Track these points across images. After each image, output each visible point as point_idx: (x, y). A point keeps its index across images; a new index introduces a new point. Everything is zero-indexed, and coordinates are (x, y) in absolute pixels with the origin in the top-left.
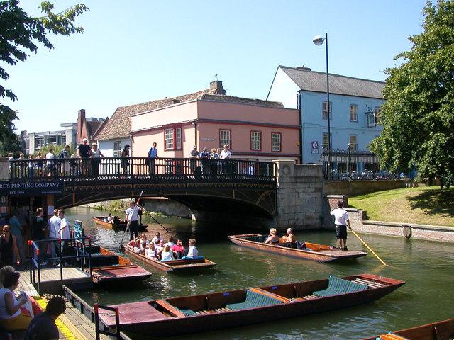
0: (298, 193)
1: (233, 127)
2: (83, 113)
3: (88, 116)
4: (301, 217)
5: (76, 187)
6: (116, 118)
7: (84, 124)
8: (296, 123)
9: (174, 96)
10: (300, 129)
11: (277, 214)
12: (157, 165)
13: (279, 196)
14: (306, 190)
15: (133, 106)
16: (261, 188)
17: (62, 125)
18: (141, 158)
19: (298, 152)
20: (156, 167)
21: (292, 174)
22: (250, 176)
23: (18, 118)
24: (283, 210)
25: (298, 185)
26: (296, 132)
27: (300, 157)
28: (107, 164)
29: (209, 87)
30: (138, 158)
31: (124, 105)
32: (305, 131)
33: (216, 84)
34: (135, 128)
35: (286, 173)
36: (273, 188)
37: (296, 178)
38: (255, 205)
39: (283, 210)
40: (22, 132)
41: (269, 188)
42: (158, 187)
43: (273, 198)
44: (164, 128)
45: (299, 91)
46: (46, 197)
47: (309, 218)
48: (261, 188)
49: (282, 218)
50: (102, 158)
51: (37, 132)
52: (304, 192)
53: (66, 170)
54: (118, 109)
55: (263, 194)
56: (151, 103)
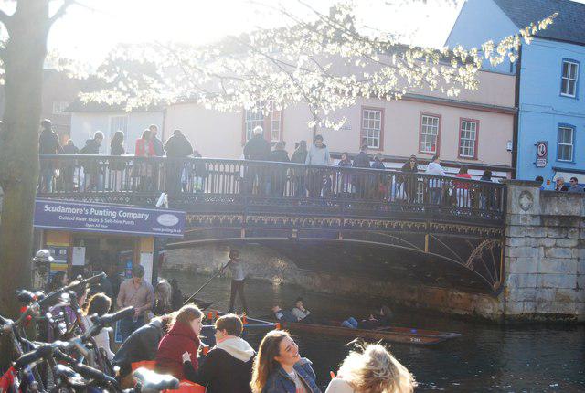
0: (545, 248)
4: (548, 295)
10: (515, 114)
13: (511, 252)
14: (560, 242)
21: (537, 210)
24: (516, 282)
25: (545, 231)
26: (509, 121)
35: (525, 205)
36: (498, 236)
37: (543, 217)
41: (491, 235)
47: (565, 300)
49: (512, 297)
52: (556, 246)
55: (481, 246)
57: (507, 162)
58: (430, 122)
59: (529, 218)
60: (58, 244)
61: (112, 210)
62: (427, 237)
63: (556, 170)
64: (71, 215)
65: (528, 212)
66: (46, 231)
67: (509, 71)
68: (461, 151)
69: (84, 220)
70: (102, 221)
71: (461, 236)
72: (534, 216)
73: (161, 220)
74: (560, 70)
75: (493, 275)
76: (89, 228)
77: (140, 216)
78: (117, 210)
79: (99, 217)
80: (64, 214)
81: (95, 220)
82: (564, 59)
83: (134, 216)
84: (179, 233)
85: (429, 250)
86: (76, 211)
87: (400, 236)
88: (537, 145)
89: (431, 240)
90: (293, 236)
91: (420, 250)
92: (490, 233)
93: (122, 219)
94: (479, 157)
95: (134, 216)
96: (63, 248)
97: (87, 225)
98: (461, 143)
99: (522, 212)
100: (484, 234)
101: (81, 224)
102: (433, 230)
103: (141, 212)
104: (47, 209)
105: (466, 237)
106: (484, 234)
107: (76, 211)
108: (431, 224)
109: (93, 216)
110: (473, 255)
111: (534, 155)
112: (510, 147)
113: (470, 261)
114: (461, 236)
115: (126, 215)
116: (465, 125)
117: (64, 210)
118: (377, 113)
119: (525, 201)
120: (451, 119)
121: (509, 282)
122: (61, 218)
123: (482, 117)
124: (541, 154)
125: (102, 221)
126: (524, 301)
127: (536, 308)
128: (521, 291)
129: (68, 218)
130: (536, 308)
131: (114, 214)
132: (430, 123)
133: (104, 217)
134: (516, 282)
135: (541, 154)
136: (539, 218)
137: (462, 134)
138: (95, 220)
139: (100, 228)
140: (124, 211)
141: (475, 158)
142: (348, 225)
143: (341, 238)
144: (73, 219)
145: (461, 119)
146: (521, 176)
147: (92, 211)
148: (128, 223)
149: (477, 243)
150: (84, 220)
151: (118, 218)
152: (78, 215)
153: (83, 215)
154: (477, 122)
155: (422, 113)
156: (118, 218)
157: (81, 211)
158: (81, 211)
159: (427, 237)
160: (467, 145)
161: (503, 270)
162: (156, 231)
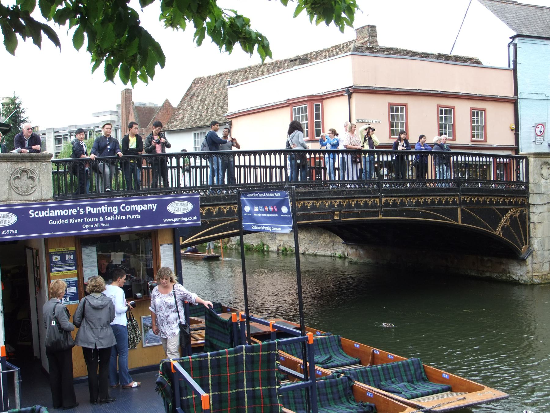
5: (384, 199)
7: (132, 111)
8: (509, 93)
9: (301, 53)
10: (514, 102)
11: (530, 252)
12: (239, 167)
13: (534, 218)
15: (220, 75)
16: (504, 203)
17: (97, 115)
19: (511, 142)
20: (169, 170)
27: (517, 150)
28: (195, 167)
31: (206, 75)
32: (522, 105)
33: (366, 31)
36: (523, 204)
38: (495, 236)
39: (542, 245)
41: (516, 204)
42: (332, 206)
43: (521, 226)
44: (289, 104)
45: (513, 38)
46: (311, 273)
48: (504, 203)
49: (539, 259)
50: (234, 153)
51: (57, 126)
53: (331, 161)
54: (195, 82)
55: (508, 214)
56: (250, 68)
57: (511, 142)
58: (445, 113)
61: (112, 205)
62: (459, 210)
64: (63, 217)
67: (507, 66)
70: (101, 219)
73: (173, 208)
75: (521, 240)
76: (87, 229)
77: (146, 207)
78: (118, 205)
79: (97, 215)
81: (93, 220)
83: (139, 208)
84: (195, 221)
86: (68, 212)
87: (436, 210)
88: (536, 127)
89: (462, 210)
90: (336, 218)
91: (454, 222)
92: (516, 202)
93: (125, 213)
94: (488, 140)
95: (139, 208)
96: (69, 253)
97: (84, 226)
98: (473, 129)
99: (543, 181)
100: (510, 203)
101: (78, 226)
102: (464, 202)
103: (147, 203)
104: (32, 214)
105: (493, 207)
106: (510, 203)
107: (68, 212)
109: (90, 215)
110: (502, 224)
111: (533, 134)
113: (499, 229)
114: (490, 207)
115: (129, 208)
117: (53, 213)
118: (402, 109)
120: (463, 110)
121: (536, 244)
122: (51, 222)
123: (488, 106)
129: (61, 222)
131: (115, 209)
132: (446, 114)
133: (103, 215)
135: (539, 134)
137: (473, 121)
138: (93, 220)
139: (101, 227)
141: (485, 141)
142: (387, 204)
143: (381, 217)
144: (66, 221)
145: (472, 109)
146: (522, 152)
147: (88, 209)
148: (132, 217)
151: (120, 213)
152: (72, 216)
153: (78, 216)
154: (405, 105)
156: (120, 213)
157: (74, 212)
158: (74, 212)
159: (459, 210)
161: (529, 236)
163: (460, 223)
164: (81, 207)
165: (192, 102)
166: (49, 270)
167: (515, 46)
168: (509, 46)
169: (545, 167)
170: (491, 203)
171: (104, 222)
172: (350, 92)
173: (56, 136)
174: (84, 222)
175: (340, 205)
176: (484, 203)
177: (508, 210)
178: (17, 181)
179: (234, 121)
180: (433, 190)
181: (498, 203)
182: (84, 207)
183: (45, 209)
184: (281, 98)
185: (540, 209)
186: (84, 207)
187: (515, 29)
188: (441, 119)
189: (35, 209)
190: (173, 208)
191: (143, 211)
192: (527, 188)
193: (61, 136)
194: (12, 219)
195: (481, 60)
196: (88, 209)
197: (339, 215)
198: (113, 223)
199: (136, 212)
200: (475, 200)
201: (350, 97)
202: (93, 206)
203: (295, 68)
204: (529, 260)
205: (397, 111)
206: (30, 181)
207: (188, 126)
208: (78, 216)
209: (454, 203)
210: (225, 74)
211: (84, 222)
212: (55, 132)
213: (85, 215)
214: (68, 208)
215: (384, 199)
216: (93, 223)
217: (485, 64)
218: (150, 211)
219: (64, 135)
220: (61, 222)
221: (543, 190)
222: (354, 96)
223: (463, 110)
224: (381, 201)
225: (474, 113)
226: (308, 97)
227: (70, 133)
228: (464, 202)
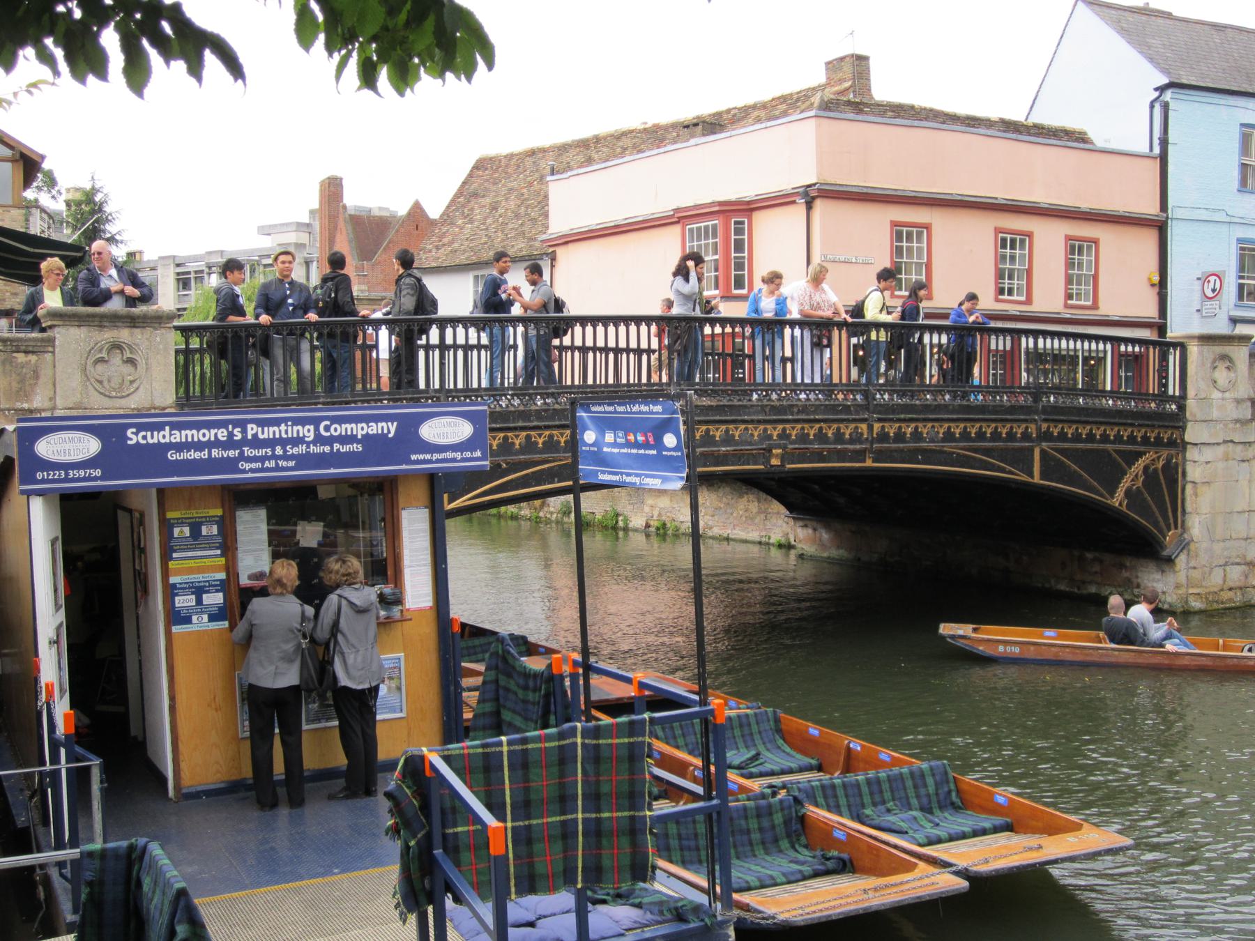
1: (938, 220)
2: (332, 189)
3: (353, 199)
6: (475, 195)
8: (1149, 207)
9: (706, 108)
10: (1161, 227)
11: (1184, 545)
13: (1194, 472)
16: (1132, 439)
17: (266, 231)
18: (638, 320)
20: (422, 354)
22: (611, 386)
23: (444, 81)
26: (1149, 240)
27: (1162, 329)
29: (821, 78)
30: (594, 320)
32: (1175, 233)
33: (847, 68)
34: (559, 224)
36: (1172, 443)
40: (131, 255)
41: (1158, 442)
43: (1166, 488)
44: (680, 218)
45: (1162, 89)
48: (1132, 439)
49: (1203, 559)
51: (182, 251)
54: (481, 165)
55: (1140, 464)
59: (1230, 406)
60: (194, 513)
61: (302, 422)
63: (1234, 321)
64: (199, 446)
65: (1227, 395)
66: (162, 492)
68: (1069, 296)
69: (233, 453)
70: (279, 451)
71: (1102, 446)
72: (1238, 401)
73: (431, 431)
74: (1235, 145)
77: (374, 429)
78: (316, 422)
80: (180, 447)
81: (262, 452)
82: (1243, 125)
83: (360, 430)
84: (478, 460)
85: (1044, 475)
87: (987, 452)
88: (1204, 279)
89: (1043, 452)
90: (775, 462)
91: (1024, 478)
93: (330, 441)
94: (1101, 304)
95: (360, 430)
98: (1069, 280)
99: (1216, 395)
100: (1146, 440)
101: (231, 465)
102: (1047, 436)
104: (133, 437)
105: (1109, 447)
106: (1146, 440)
108: (877, 426)
109: (256, 442)
111: (1197, 296)
112: (1156, 279)
113: (1120, 493)
114: (1102, 446)
116: (1074, 247)
117: (178, 437)
118: (919, 235)
119: (1222, 375)
120: (1049, 241)
122: (172, 456)
124: (1210, 294)
125: (279, 451)
126: (1226, 564)
127: (1246, 577)
128: (1218, 547)
129: (193, 455)
130: (1246, 577)
131: (308, 432)
132: (1013, 247)
133: (283, 442)
134: (1210, 530)
135: (1210, 294)
136: (1249, 404)
137: (1069, 264)
138: (262, 452)
139: (277, 468)
140: (335, 420)
141: (1095, 306)
143: (869, 463)
144: (204, 455)
147: (252, 429)
149: (1132, 457)
150: (233, 453)
151: (319, 439)
152: (216, 443)
153: (230, 443)
154: (928, 227)
155: (998, 230)
157: (222, 434)
158: (222, 434)
160: (1079, 284)
162: (420, 461)
163: (1037, 479)
164: (236, 423)
165: (472, 210)
166: (166, 556)
167: (1166, 107)
168: (1152, 107)
169: (1222, 366)
170: (1105, 439)
171: (286, 457)
172: (810, 196)
173: (178, 274)
174: (242, 457)
175: (784, 435)
176: (1091, 438)
177: (1140, 455)
178: (100, 367)
179: (560, 252)
180: (982, 409)
181: (1118, 439)
182: (242, 425)
183: (159, 427)
184: (664, 206)
185: (1208, 454)
186: (242, 425)
187: (1165, 71)
188: (1004, 257)
189: (140, 428)
190: (431, 431)
191: (367, 437)
192: (1182, 408)
193: (189, 273)
194: (90, 446)
195: (1091, 135)
196: (252, 429)
197: (783, 458)
198: (304, 461)
199: (351, 439)
200: (1112, 434)
201: (809, 206)
202: (262, 423)
203: (693, 141)
204: (1181, 561)
205: (909, 237)
206: (128, 369)
207: (462, 259)
208: (230, 443)
209: (1026, 436)
210: (543, 150)
211: (242, 457)
212: (178, 265)
213: (244, 442)
214: (209, 425)
215: (877, 426)
216: (262, 459)
217: (1099, 143)
218: (383, 437)
219: (196, 272)
220: (193, 455)
221: (1215, 414)
222: (819, 205)
223: (1049, 241)
224: (871, 428)
225: (1073, 247)
226: (720, 204)
227: (210, 268)
228: (1047, 436)
